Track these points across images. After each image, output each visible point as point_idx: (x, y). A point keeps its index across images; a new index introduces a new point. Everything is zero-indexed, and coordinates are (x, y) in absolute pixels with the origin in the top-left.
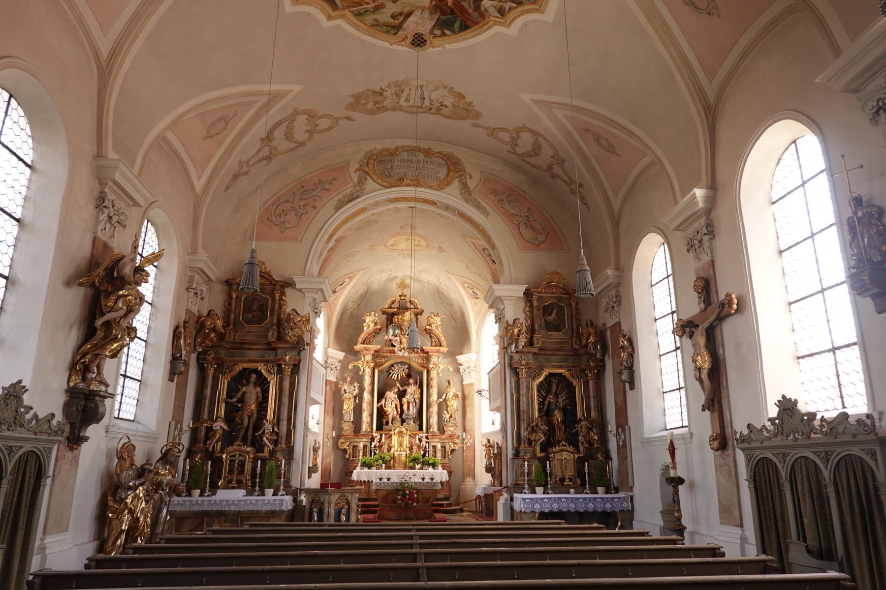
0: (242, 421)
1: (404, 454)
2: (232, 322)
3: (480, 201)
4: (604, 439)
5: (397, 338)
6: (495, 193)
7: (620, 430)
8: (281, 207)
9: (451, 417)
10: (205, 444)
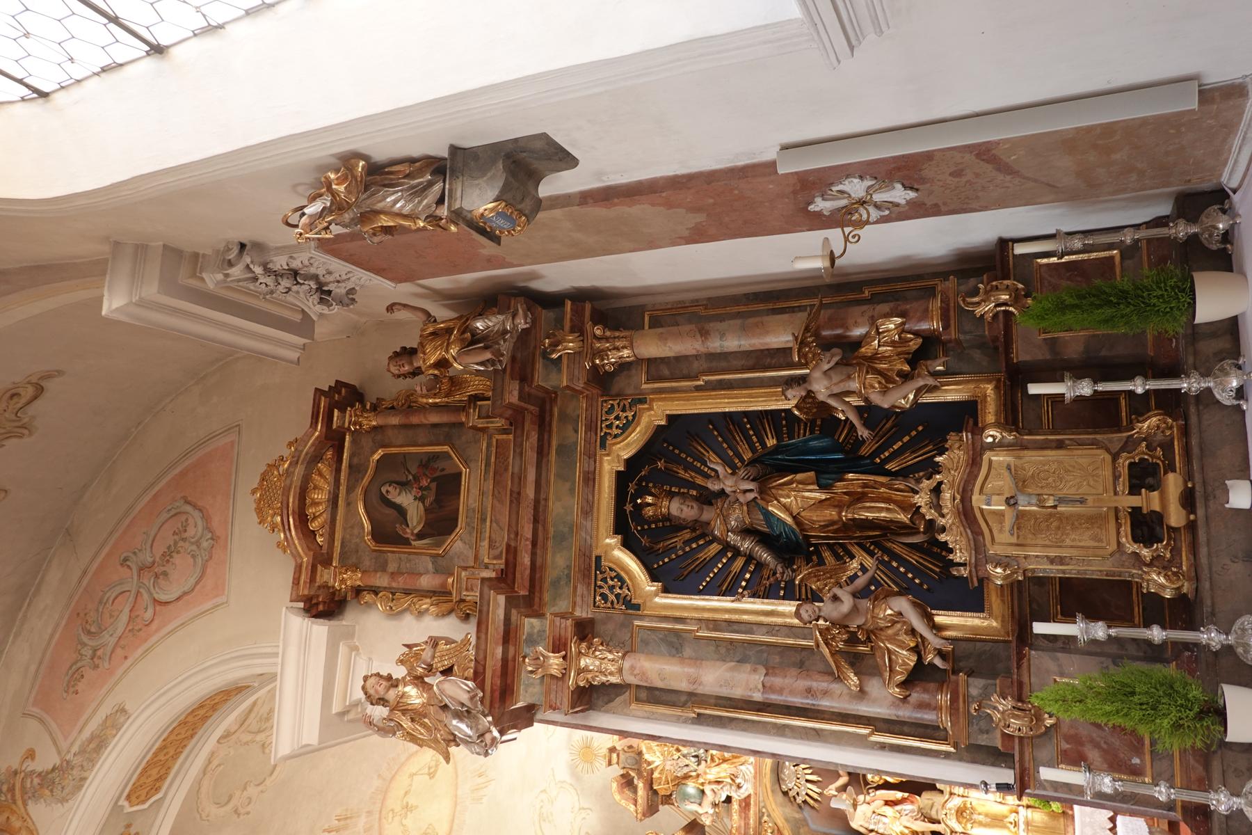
3: (86, 734)
4: (898, 286)
5: (707, 789)
6: (75, 676)
7: (821, 205)
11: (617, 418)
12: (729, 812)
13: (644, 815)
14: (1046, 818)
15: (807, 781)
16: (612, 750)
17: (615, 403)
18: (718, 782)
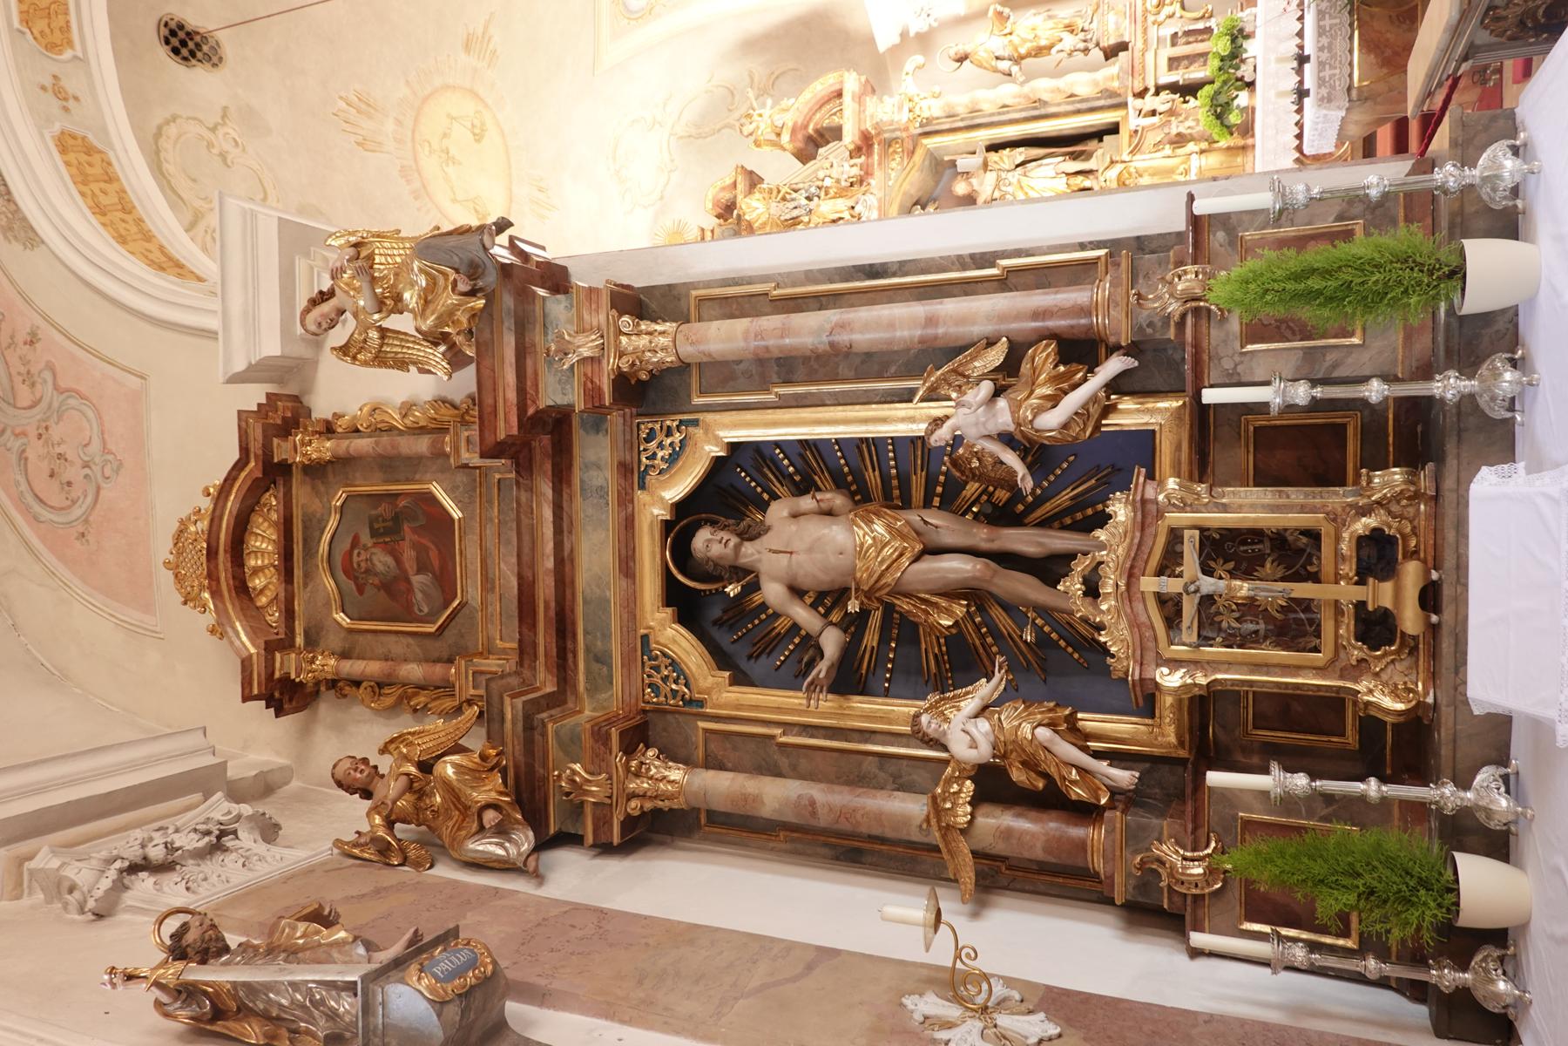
0: (953, 593)
1: (1195, 162)
2: (438, 670)
8: (42, 485)
9: (1070, 29)
10: (1087, 812)
11: (661, 446)
17: (657, 427)
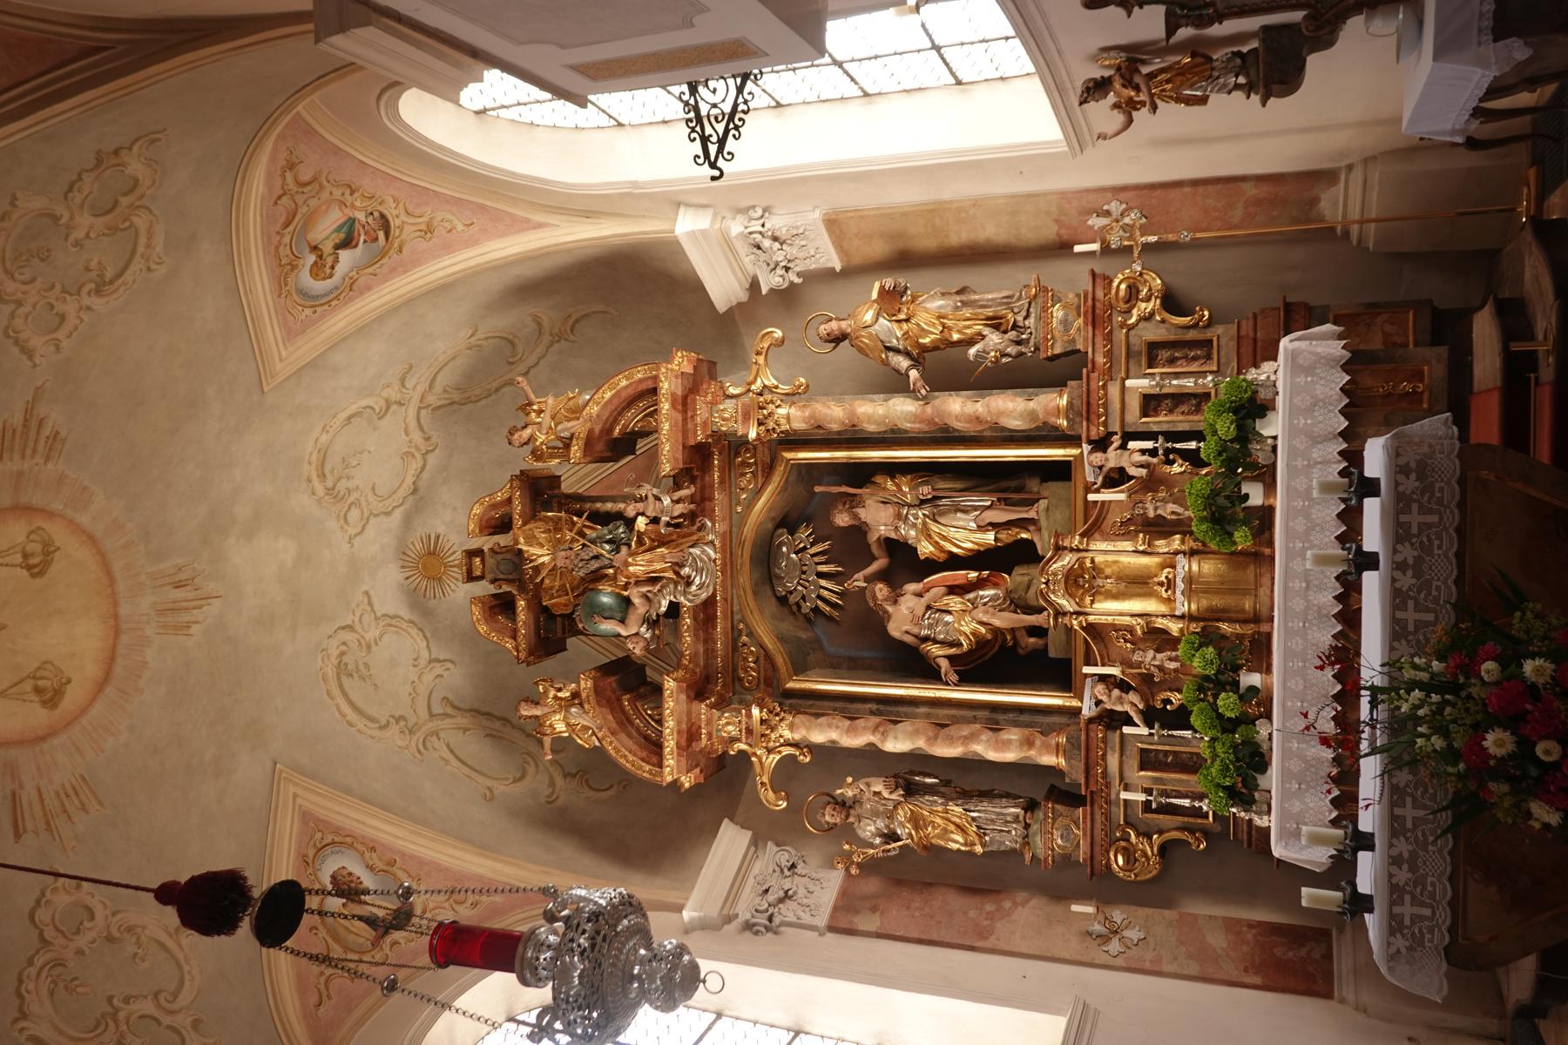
5: (635, 595)
12: (677, 635)
13: (530, 653)
14: (1222, 567)
15: (820, 575)
16: (471, 554)
18: (653, 581)
